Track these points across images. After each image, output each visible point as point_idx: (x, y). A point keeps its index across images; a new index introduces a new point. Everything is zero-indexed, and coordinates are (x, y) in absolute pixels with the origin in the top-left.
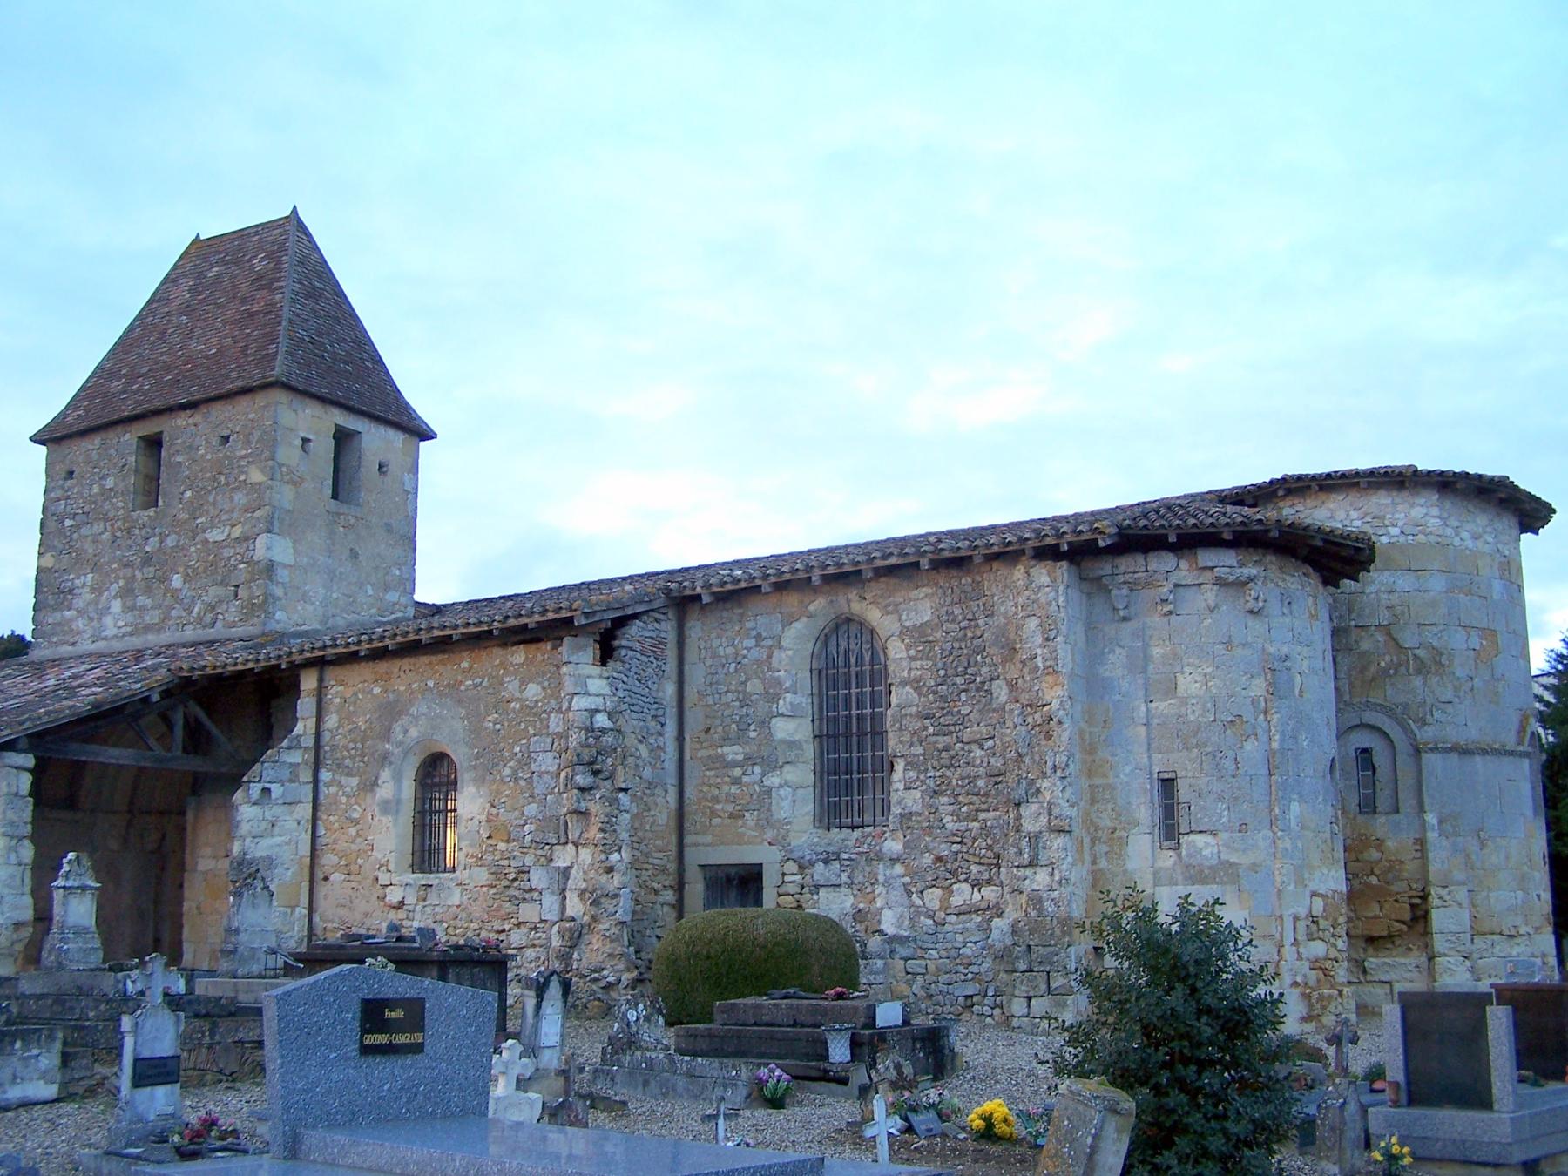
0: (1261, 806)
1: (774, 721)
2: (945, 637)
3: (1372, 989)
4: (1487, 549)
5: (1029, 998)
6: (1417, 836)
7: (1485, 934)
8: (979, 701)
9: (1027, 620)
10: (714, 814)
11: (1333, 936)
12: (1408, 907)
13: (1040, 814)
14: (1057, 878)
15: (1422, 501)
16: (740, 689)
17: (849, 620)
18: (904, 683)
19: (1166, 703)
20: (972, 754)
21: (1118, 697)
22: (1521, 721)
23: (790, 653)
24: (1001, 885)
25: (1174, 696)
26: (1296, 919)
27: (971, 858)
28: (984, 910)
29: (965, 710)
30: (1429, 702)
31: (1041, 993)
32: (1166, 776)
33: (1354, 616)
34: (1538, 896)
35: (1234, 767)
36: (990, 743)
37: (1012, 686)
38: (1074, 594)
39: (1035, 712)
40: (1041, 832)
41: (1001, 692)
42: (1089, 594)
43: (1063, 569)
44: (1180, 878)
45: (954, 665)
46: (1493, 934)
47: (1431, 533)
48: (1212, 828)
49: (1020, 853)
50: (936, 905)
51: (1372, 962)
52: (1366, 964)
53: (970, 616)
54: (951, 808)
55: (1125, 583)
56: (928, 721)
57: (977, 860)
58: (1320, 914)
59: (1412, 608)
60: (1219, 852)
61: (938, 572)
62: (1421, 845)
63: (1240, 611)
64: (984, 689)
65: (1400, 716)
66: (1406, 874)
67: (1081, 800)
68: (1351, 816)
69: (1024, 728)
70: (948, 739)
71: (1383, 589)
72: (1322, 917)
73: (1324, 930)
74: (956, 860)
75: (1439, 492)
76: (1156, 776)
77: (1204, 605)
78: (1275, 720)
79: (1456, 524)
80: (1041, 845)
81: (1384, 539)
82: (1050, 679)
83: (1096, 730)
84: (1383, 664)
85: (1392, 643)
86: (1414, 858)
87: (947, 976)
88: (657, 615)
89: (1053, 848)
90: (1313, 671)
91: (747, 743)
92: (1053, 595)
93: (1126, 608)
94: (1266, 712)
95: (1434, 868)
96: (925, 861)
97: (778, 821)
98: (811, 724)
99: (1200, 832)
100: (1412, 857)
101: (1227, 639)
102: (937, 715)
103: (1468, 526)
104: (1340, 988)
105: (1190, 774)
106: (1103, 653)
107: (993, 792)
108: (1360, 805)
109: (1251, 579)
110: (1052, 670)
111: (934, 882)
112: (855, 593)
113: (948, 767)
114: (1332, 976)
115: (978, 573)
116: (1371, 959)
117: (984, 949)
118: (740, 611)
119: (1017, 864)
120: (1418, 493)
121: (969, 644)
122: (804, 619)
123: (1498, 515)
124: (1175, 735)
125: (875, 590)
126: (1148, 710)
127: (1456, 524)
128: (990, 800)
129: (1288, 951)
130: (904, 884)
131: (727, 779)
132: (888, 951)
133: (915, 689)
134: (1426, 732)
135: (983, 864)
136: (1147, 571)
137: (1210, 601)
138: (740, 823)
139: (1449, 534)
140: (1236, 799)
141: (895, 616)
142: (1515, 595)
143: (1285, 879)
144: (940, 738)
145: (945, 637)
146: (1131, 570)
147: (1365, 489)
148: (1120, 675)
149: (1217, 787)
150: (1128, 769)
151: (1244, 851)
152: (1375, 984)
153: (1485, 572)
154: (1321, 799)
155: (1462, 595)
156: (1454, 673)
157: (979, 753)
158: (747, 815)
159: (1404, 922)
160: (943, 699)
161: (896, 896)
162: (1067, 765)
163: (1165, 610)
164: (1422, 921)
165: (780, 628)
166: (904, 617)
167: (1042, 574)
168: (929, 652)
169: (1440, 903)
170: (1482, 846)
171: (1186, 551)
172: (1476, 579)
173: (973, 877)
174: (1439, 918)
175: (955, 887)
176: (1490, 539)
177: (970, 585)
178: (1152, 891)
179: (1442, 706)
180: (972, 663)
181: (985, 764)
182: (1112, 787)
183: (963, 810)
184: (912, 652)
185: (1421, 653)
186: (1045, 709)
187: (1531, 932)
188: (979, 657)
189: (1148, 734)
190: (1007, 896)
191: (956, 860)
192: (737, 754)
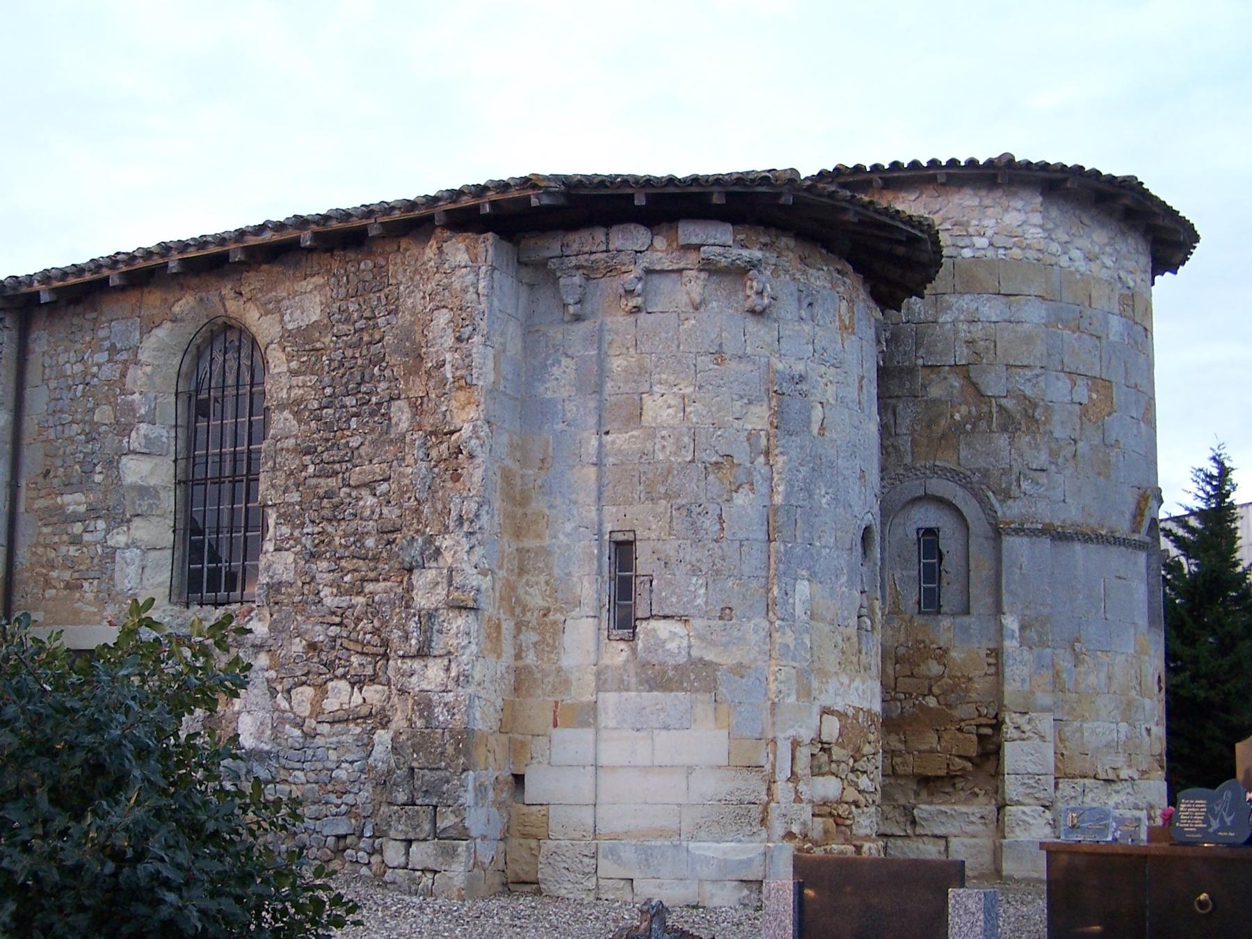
0: (754, 584)
1: (124, 459)
2: (336, 343)
3: (921, 846)
4: (1104, 274)
5: (409, 842)
6: (992, 646)
7: (1074, 777)
8: (372, 430)
9: (436, 313)
10: (48, 583)
11: (853, 770)
12: (974, 738)
13: (437, 584)
14: (453, 674)
15: (1019, 204)
16: (86, 418)
17: (227, 327)
18: (282, 407)
19: (627, 436)
20: (361, 503)
21: (560, 426)
22: (1139, 503)
23: (148, 369)
24: (389, 684)
25: (639, 426)
26: (796, 744)
27: (351, 646)
28: (365, 718)
29: (354, 442)
30: (1016, 470)
31: (422, 836)
32: (620, 537)
33: (921, 352)
34: (1148, 730)
35: (718, 526)
36: (384, 487)
37: (417, 408)
38: (506, 281)
39: (441, 443)
40: (437, 610)
41: (401, 416)
42: (531, 286)
43: (487, 244)
44: (633, 680)
45: (344, 380)
46: (1085, 777)
47: (1029, 247)
48: (682, 612)
49: (406, 637)
50: (304, 710)
51: (923, 810)
52: (915, 812)
53: (367, 314)
54: (331, 576)
55: (578, 267)
56: (308, 457)
57: (359, 649)
58: (834, 741)
59: (998, 346)
60: (690, 647)
61: (332, 256)
62: (997, 657)
63: (737, 310)
64: (380, 412)
65: (976, 486)
66: (974, 695)
67: (501, 568)
68: (907, 617)
69: (424, 464)
70: (332, 482)
71: (962, 317)
72: (836, 744)
73: (838, 762)
74: (333, 648)
75: (1042, 194)
76: (607, 537)
77: (685, 299)
78: (779, 465)
79: (1065, 238)
80: (435, 628)
81: (967, 253)
82: (462, 396)
83: (531, 472)
84: (957, 417)
85: (971, 390)
86: (986, 674)
87: (314, 808)
88: (600, 580)
89: (452, 632)
90: (841, 400)
91: (91, 489)
92: (471, 278)
93: (579, 302)
94: (767, 453)
95: (1011, 688)
96: (294, 648)
97: (121, 593)
98: (173, 465)
99: (665, 617)
100: (982, 673)
101: (717, 348)
102: (319, 448)
103: (1079, 242)
104: (858, 843)
105: (653, 536)
106: (544, 366)
107: (385, 555)
108: (919, 603)
109: (753, 265)
110: (462, 383)
111: (304, 678)
112: (229, 287)
113: (330, 521)
114: (849, 826)
115: (381, 254)
116: (922, 806)
117: (362, 771)
118: (94, 315)
119: (401, 653)
120: (1015, 194)
121: (364, 352)
122: (168, 325)
123: (1123, 233)
124: (636, 480)
125: (253, 281)
126: (601, 445)
127: (1065, 238)
128: (381, 566)
129: (783, 790)
130: (268, 681)
131: (65, 538)
132: (244, 770)
133: (296, 414)
134: (1010, 508)
135: (367, 654)
136: (607, 251)
137: (693, 295)
138: (78, 595)
139: (1054, 250)
140: (718, 572)
141: (277, 316)
142: (1140, 340)
143: (782, 687)
144: (322, 481)
145: (336, 343)
146: (586, 249)
147: (944, 185)
148: (566, 395)
149: (691, 555)
150: (569, 527)
151: (726, 645)
152: (925, 839)
153: (1100, 303)
154: (844, 579)
155: (1067, 332)
156: (1051, 433)
157: (370, 501)
158: (86, 585)
159: (969, 759)
160: (328, 426)
161: (256, 696)
162: (477, 516)
163: (631, 304)
164: (993, 758)
165: (138, 337)
166: (287, 318)
167: (458, 250)
168: (315, 364)
169: (1016, 734)
170: (1077, 660)
171: (665, 226)
172: (1088, 312)
173: (352, 672)
174: (1014, 755)
175: (330, 684)
176: (1109, 263)
177: (371, 271)
178: (593, 698)
179: (1032, 474)
180: (367, 377)
181: (376, 517)
182: (548, 552)
183: (346, 579)
184: (294, 365)
185: (1009, 403)
186: (453, 438)
187: (1136, 777)
188: (376, 369)
189: (599, 478)
190: (395, 699)
191: (333, 648)
192: (79, 504)
